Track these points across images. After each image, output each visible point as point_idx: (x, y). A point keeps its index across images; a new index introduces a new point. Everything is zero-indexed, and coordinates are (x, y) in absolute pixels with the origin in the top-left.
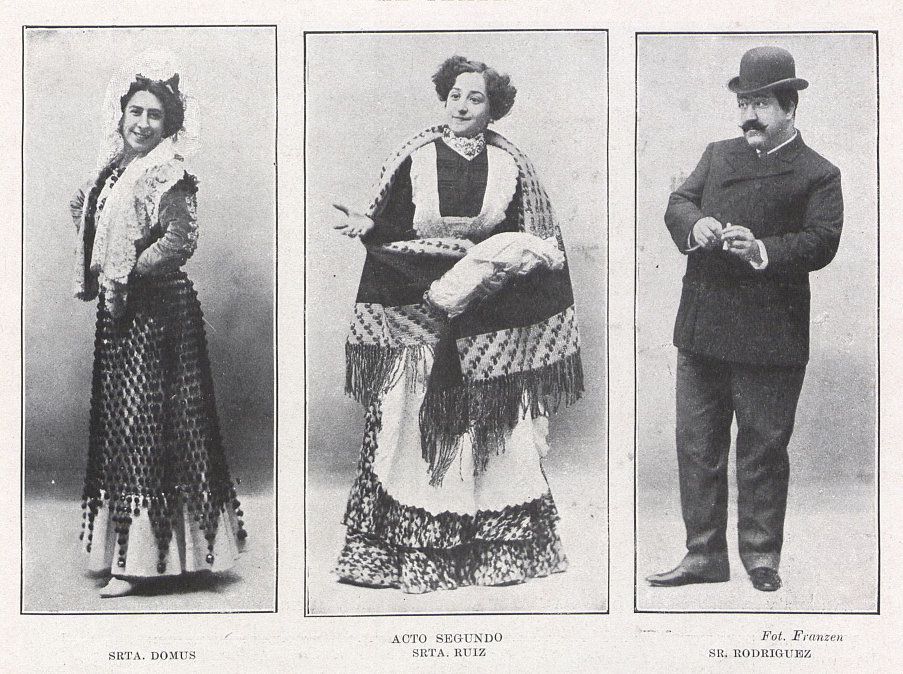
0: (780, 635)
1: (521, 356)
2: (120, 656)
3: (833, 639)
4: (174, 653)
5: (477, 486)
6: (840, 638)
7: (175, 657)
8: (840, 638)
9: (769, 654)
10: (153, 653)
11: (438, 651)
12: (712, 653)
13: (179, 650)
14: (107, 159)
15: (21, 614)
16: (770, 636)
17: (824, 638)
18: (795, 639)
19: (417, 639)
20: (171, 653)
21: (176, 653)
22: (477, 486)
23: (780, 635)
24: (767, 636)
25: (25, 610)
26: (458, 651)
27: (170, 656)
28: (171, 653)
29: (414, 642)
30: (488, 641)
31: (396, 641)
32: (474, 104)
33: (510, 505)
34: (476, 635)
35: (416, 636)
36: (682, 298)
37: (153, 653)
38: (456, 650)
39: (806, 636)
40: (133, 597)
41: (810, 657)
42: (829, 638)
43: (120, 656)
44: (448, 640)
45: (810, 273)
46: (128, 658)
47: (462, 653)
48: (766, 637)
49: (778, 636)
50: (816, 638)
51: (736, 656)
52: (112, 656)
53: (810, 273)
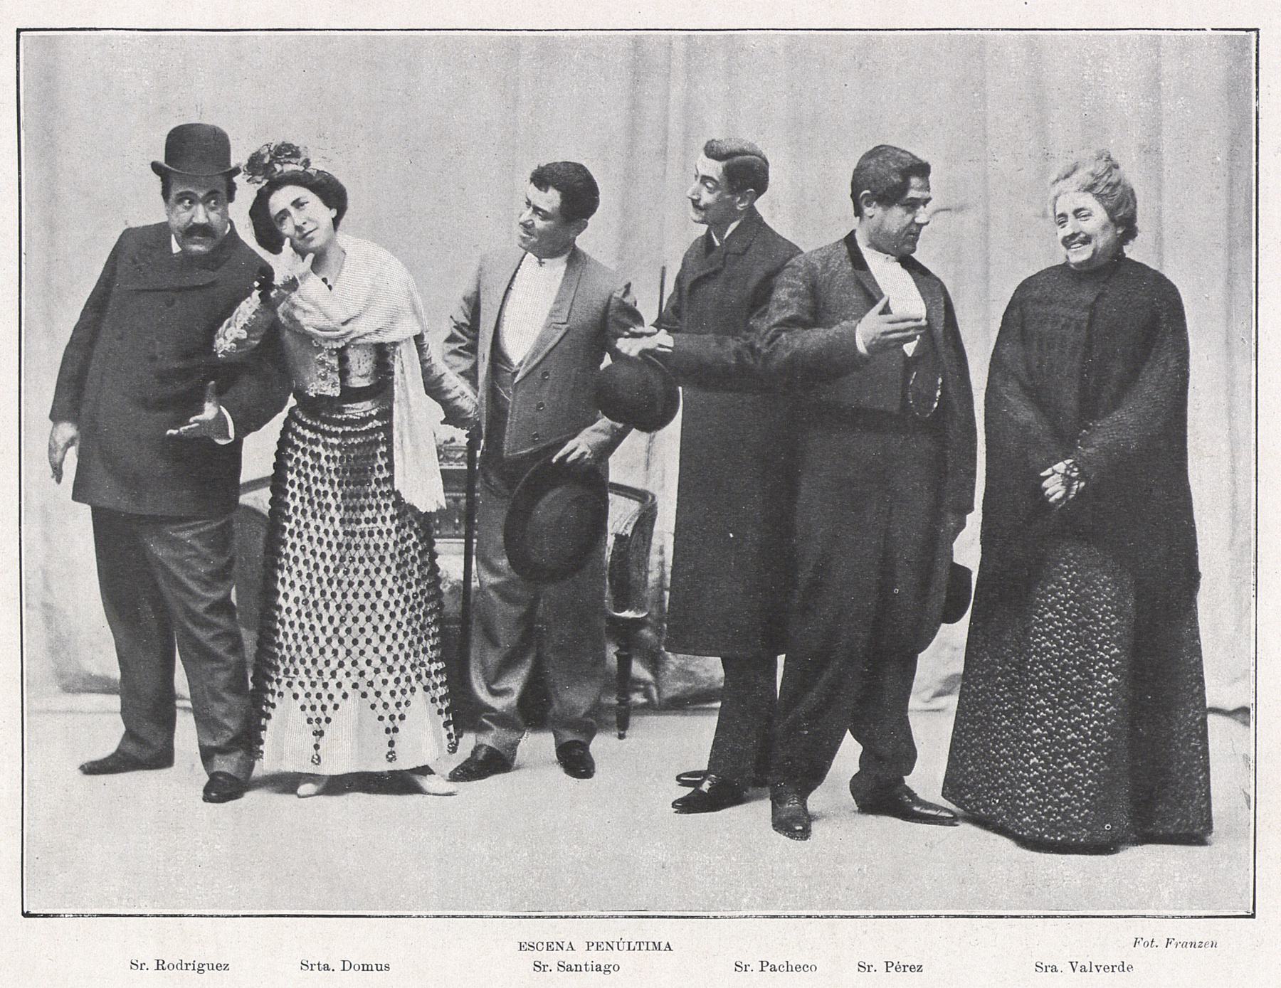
4: (657, 944)
8: (1214, 945)
12: (226, 967)
16: (1142, 943)
17: (1197, 945)
20: (654, 943)
26: (161, 962)
28: (654, 943)
34: (557, 943)
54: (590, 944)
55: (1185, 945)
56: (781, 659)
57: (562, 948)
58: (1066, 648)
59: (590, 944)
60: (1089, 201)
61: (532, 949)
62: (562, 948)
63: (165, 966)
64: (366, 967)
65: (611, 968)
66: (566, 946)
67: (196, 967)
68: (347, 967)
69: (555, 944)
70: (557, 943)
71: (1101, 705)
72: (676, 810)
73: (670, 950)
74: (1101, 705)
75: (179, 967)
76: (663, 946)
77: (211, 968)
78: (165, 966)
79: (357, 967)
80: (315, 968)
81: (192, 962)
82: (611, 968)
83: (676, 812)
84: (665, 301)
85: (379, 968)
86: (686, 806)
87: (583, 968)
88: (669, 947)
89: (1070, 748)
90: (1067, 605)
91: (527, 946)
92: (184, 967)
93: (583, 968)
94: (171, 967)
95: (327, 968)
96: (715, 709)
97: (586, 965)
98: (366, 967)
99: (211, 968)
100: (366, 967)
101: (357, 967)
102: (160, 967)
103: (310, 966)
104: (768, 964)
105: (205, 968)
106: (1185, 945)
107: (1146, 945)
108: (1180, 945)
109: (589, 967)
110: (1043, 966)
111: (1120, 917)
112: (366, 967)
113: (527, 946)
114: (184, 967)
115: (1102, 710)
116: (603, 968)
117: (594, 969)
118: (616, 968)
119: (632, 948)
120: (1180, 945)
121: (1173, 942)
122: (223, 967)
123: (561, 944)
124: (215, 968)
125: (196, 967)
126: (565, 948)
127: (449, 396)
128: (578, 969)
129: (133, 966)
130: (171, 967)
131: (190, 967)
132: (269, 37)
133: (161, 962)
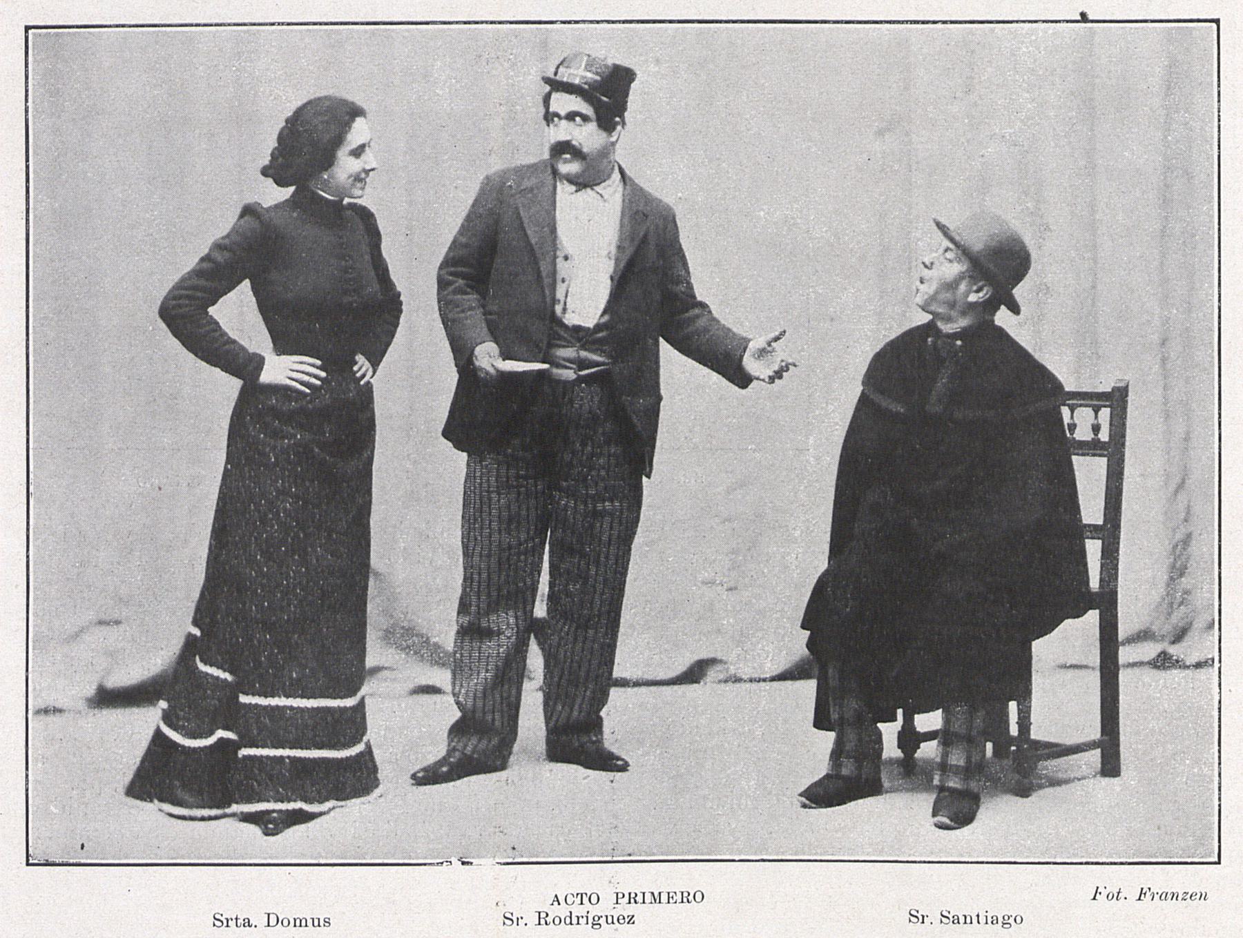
0: (1119, 893)
2: (316, 923)
3: (1193, 898)
5: (444, 692)
6: (1204, 897)
7: (658, 901)
8: (1204, 897)
9: (679, 898)
10: (269, 915)
12: (327, 922)
13: (665, 889)
14: (94, 715)
15: (27, 28)
17: (1180, 898)
18: (1139, 899)
19: (585, 900)
20: (653, 893)
21: (660, 893)
22: (444, 692)
23: (1119, 893)
24: (1145, 894)
25: (34, 34)
26: (543, 915)
27: (648, 898)
28: (653, 893)
29: (582, 904)
30: (271, 924)
33: (780, 381)
35: (584, 895)
37: (269, 915)
38: (660, 902)
39: (1156, 895)
40: (618, 228)
41: (633, 923)
42: (1189, 896)
43: (316, 923)
44: (671, 899)
47: (640, 899)
48: (1143, 895)
50: (1169, 896)
51: (987, 923)
52: (327, 922)
55: (1164, 896)
56: (244, 699)
63: (549, 919)
64: (299, 923)
65: (602, 921)
67: (590, 921)
68: (273, 921)
72: (414, 782)
75: (568, 920)
77: (610, 921)
78: (549, 919)
79: (285, 923)
80: (232, 923)
81: (234, 917)
82: (1011, 921)
83: (413, 784)
85: (316, 923)
86: (624, 768)
87: (975, 920)
88: (558, 901)
92: (575, 921)
93: (975, 920)
94: (557, 921)
95: (248, 923)
96: (1130, 640)
97: (978, 916)
98: (298, 922)
99: (610, 921)
100: (298, 922)
101: (285, 923)
103: (921, 918)
104: (244, 926)
105: (602, 921)
106: (1164, 896)
108: (1157, 897)
109: (982, 920)
110: (950, 916)
111: (925, 862)
112: (299, 923)
114: (575, 921)
116: (1000, 920)
117: (989, 921)
118: (1019, 920)
119: (579, 896)
120: (1157, 897)
121: (1148, 894)
122: (627, 920)
124: (615, 921)
125: (590, 921)
128: (968, 920)
129: (507, 921)
130: (557, 921)
131: (583, 921)
132: (1209, 158)
133: (685, 894)
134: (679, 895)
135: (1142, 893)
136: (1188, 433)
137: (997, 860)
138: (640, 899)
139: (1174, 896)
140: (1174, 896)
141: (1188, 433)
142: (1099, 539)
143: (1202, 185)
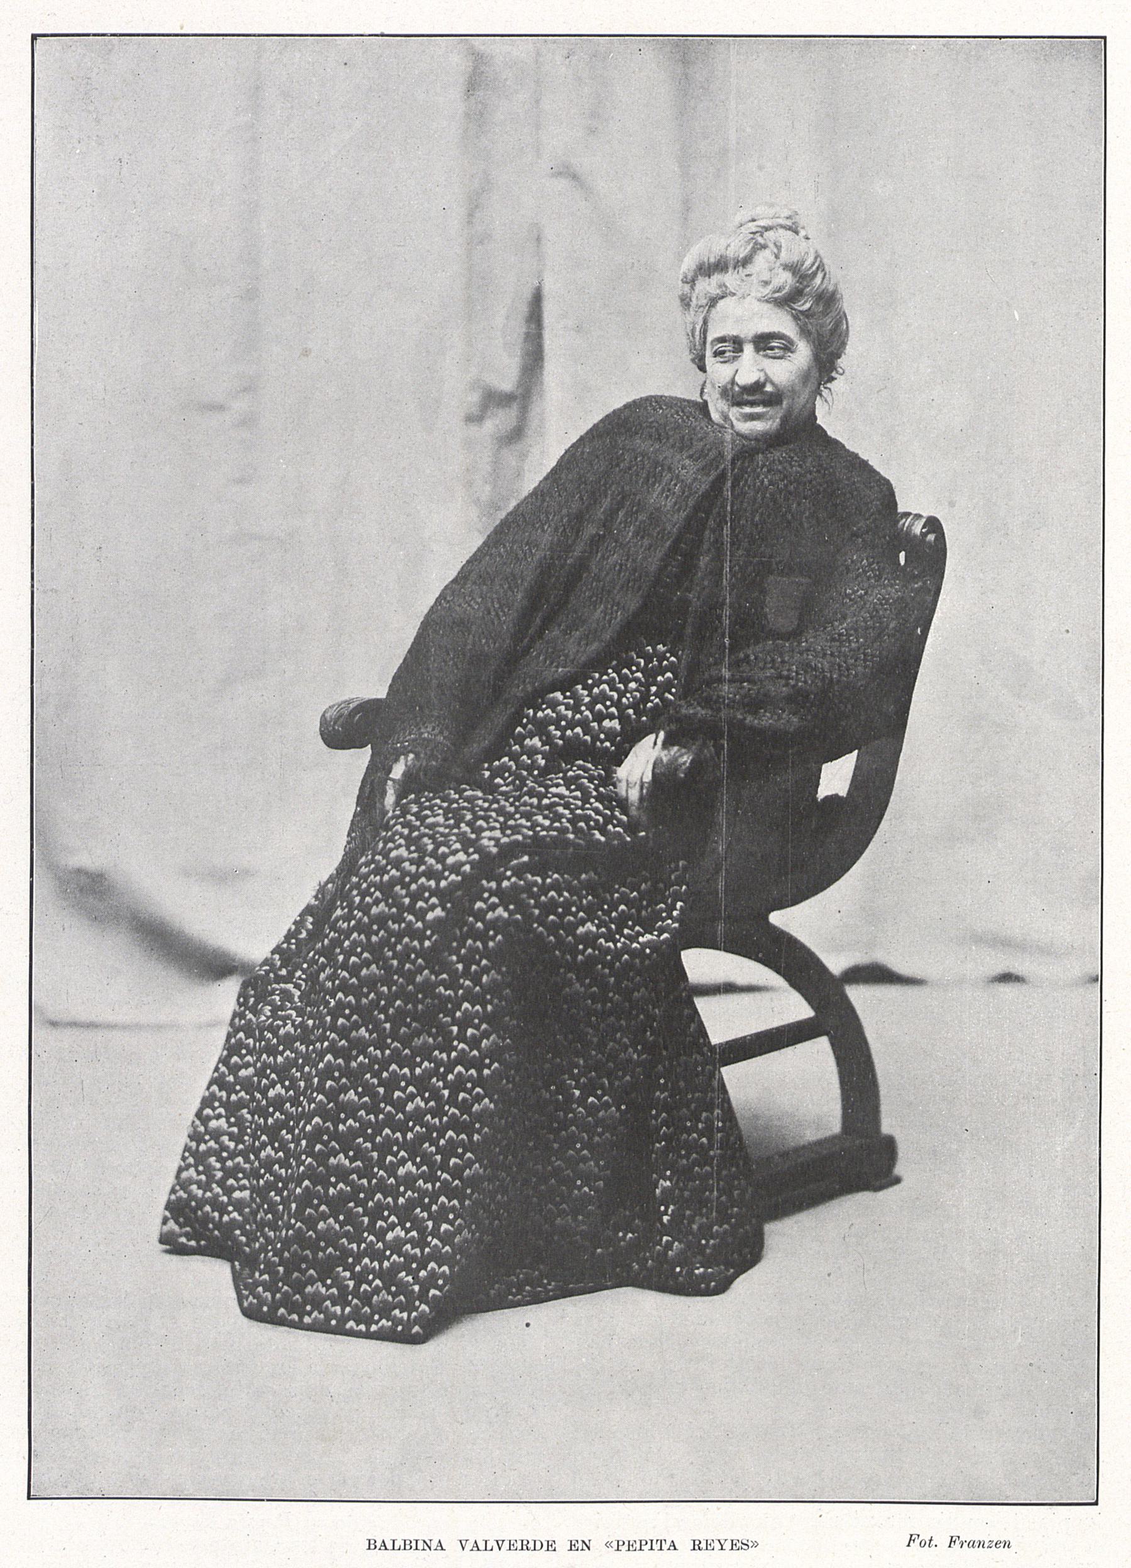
0: (931, 1540)
1: (560, 788)
11: (669, 1543)
16: (917, 1542)
17: (986, 1545)
23: (931, 1540)
26: (697, 1543)
31: (672, 1548)
32: (165, 1239)
34: (583, 1542)
36: (410, 651)
44: (550, 1548)
45: (682, 953)
46: (661, 1549)
47: (531, 1546)
49: (928, 1543)
50: (976, 1544)
53: (682, 953)
54: (621, 1543)
55: (972, 1544)
57: (430, 1548)
58: (540, 925)
59: (621, 1543)
60: (781, 323)
61: (746, 1547)
62: (430, 1548)
66: (434, 1545)
69: (580, 1542)
70: (424, 1541)
71: (470, 1031)
73: (675, 1549)
74: (470, 1031)
76: (434, 1545)
84: (844, 322)
88: (385, 1546)
89: (344, 1122)
90: (355, 892)
91: (739, 1545)
102: (697, 1547)
106: (972, 1544)
107: (922, 1545)
113: (739, 1545)
115: (475, 1043)
119: (489, 1548)
120: (965, 1545)
121: (957, 1542)
123: (428, 1542)
126: (433, 1547)
127: (825, 393)
134: (519, 1543)
135: (911, 1539)
136: (750, 221)
137: (36, 342)
138: (531, 1546)
139: (981, 1544)
140: (981, 1544)
141: (750, 221)
142: (720, 1072)
143: (623, 525)
